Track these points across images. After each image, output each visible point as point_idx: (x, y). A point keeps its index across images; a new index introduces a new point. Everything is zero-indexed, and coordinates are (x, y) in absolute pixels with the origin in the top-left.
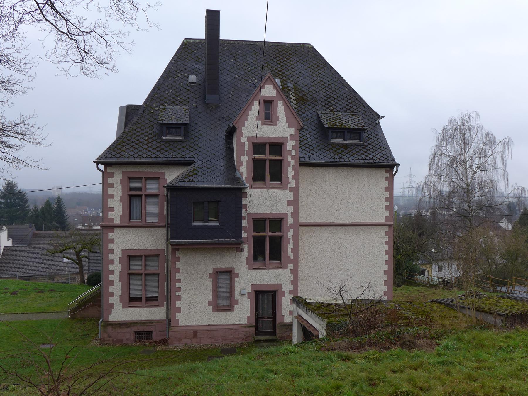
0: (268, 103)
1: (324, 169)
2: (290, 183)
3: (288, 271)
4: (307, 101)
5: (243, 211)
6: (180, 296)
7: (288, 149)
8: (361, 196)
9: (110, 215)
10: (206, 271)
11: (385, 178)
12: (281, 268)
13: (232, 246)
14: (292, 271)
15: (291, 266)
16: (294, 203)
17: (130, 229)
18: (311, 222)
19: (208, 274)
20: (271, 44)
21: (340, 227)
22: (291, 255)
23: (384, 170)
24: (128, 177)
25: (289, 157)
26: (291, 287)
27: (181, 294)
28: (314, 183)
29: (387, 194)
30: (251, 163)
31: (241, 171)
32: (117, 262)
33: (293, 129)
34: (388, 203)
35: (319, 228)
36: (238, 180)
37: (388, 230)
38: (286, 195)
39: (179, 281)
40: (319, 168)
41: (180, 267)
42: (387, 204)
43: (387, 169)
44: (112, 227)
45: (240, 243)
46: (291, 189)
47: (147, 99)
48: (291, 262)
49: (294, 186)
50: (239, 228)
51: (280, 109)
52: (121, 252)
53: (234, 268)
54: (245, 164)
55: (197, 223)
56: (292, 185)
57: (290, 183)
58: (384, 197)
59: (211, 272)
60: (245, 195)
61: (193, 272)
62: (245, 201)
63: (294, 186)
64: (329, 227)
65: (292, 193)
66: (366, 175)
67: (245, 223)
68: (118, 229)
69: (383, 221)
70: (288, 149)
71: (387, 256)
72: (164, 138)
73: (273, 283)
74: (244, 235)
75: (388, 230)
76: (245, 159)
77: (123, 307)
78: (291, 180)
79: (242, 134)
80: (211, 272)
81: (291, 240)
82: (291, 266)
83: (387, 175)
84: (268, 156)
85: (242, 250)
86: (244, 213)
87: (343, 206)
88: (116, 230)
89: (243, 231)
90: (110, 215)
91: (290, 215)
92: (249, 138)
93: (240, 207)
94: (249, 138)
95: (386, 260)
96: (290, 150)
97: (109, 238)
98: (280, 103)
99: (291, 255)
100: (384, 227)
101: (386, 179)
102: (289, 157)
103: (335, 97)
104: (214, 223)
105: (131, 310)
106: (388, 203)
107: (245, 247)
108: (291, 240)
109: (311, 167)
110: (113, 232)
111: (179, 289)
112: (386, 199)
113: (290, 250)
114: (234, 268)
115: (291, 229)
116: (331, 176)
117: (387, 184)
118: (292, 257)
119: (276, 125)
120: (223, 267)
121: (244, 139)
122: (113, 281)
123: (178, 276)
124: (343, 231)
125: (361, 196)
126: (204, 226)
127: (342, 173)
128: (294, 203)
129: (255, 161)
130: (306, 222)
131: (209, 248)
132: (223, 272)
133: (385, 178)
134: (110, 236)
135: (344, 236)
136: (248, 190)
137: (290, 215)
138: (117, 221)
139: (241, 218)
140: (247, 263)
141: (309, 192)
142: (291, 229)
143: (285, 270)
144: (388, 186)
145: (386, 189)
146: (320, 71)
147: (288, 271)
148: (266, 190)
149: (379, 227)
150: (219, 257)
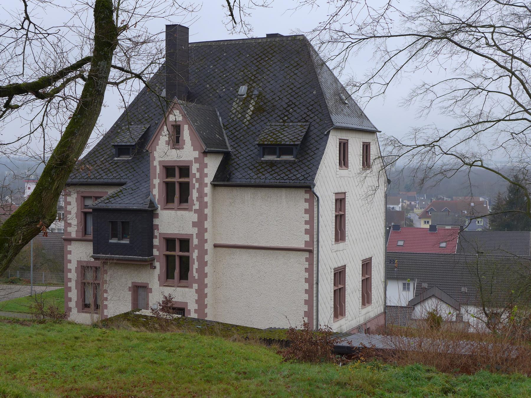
0: (177, 129)
1: (242, 189)
2: (195, 205)
3: (193, 291)
4: (264, 111)
5: (156, 231)
6: (107, 305)
7: (193, 172)
8: (279, 218)
9: (69, 229)
10: (126, 284)
11: (305, 199)
12: (187, 287)
13: (146, 263)
14: (197, 291)
15: (195, 286)
16: (199, 224)
17: (83, 242)
18: (230, 243)
19: (128, 287)
20: (260, 41)
21: (259, 250)
22: (196, 275)
23: (304, 191)
24: (82, 196)
25: (194, 179)
26: (196, 307)
27: (108, 304)
28: (233, 204)
29: (307, 217)
30: (164, 187)
31: (154, 193)
32: (73, 271)
33: (197, 152)
34: (308, 227)
35: (238, 250)
36: (152, 203)
37: (308, 256)
38: (191, 216)
39: (106, 291)
40: (238, 188)
41: (72, 277)
42: (307, 228)
43: (308, 189)
44: (70, 240)
45: (153, 260)
46: (196, 211)
47: (120, 118)
48: (196, 281)
49: (198, 208)
50: (151, 246)
51: (186, 133)
52: (76, 262)
53: (148, 284)
54: (157, 186)
55: (114, 241)
56: (196, 206)
57: (195, 205)
58: (304, 220)
59: (130, 286)
60: (157, 216)
61: (117, 284)
62: (156, 222)
63: (198, 208)
64: (248, 250)
65: (196, 215)
66: (285, 196)
67: (156, 242)
68: (74, 242)
69: (302, 246)
70: (193, 172)
71: (307, 284)
72: (116, 159)
73: (180, 301)
74: (156, 252)
75: (308, 256)
76: (156, 182)
77: (78, 312)
78: (195, 202)
79: (154, 159)
80: (130, 286)
81: (196, 260)
82: (195, 286)
83: (307, 196)
84: (177, 179)
85: (155, 268)
86: (156, 233)
87: (261, 228)
88: (73, 242)
89: (154, 250)
90: (69, 229)
91: (195, 236)
92: (160, 162)
93: (151, 228)
94: (160, 162)
95: (306, 288)
96: (195, 172)
97: (68, 249)
98: (186, 127)
99: (196, 275)
100: (304, 253)
101: (306, 200)
102: (194, 179)
103: (297, 104)
104: (126, 241)
105: (84, 315)
106: (308, 227)
107: (157, 264)
108: (196, 260)
109: (230, 188)
110: (71, 245)
111: (106, 299)
112: (306, 223)
113: (194, 270)
114: (148, 284)
115: (195, 250)
116: (249, 197)
117: (307, 205)
118: (196, 278)
119: (183, 148)
120: (140, 282)
121: (156, 163)
122: (71, 287)
123: (105, 287)
124: (261, 254)
125: (279, 218)
126: (118, 243)
127: (261, 193)
128: (199, 224)
129: (167, 184)
130: (226, 243)
131: (129, 264)
132: (141, 287)
133: (305, 199)
134: (69, 248)
135: (263, 259)
136: (159, 211)
137: (195, 236)
138: (74, 235)
139: (151, 237)
140: (159, 280)
141: (229, 213)
142: (195, 250)
143: (191, 290)
144: (308, 208)
145: (306, 211)
146: (296, 72)
147: (193, 291)
148: (174, 211)
149: (299, 253)
150: (136, 272)
